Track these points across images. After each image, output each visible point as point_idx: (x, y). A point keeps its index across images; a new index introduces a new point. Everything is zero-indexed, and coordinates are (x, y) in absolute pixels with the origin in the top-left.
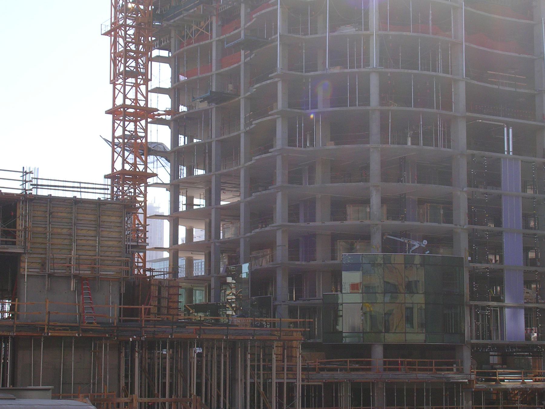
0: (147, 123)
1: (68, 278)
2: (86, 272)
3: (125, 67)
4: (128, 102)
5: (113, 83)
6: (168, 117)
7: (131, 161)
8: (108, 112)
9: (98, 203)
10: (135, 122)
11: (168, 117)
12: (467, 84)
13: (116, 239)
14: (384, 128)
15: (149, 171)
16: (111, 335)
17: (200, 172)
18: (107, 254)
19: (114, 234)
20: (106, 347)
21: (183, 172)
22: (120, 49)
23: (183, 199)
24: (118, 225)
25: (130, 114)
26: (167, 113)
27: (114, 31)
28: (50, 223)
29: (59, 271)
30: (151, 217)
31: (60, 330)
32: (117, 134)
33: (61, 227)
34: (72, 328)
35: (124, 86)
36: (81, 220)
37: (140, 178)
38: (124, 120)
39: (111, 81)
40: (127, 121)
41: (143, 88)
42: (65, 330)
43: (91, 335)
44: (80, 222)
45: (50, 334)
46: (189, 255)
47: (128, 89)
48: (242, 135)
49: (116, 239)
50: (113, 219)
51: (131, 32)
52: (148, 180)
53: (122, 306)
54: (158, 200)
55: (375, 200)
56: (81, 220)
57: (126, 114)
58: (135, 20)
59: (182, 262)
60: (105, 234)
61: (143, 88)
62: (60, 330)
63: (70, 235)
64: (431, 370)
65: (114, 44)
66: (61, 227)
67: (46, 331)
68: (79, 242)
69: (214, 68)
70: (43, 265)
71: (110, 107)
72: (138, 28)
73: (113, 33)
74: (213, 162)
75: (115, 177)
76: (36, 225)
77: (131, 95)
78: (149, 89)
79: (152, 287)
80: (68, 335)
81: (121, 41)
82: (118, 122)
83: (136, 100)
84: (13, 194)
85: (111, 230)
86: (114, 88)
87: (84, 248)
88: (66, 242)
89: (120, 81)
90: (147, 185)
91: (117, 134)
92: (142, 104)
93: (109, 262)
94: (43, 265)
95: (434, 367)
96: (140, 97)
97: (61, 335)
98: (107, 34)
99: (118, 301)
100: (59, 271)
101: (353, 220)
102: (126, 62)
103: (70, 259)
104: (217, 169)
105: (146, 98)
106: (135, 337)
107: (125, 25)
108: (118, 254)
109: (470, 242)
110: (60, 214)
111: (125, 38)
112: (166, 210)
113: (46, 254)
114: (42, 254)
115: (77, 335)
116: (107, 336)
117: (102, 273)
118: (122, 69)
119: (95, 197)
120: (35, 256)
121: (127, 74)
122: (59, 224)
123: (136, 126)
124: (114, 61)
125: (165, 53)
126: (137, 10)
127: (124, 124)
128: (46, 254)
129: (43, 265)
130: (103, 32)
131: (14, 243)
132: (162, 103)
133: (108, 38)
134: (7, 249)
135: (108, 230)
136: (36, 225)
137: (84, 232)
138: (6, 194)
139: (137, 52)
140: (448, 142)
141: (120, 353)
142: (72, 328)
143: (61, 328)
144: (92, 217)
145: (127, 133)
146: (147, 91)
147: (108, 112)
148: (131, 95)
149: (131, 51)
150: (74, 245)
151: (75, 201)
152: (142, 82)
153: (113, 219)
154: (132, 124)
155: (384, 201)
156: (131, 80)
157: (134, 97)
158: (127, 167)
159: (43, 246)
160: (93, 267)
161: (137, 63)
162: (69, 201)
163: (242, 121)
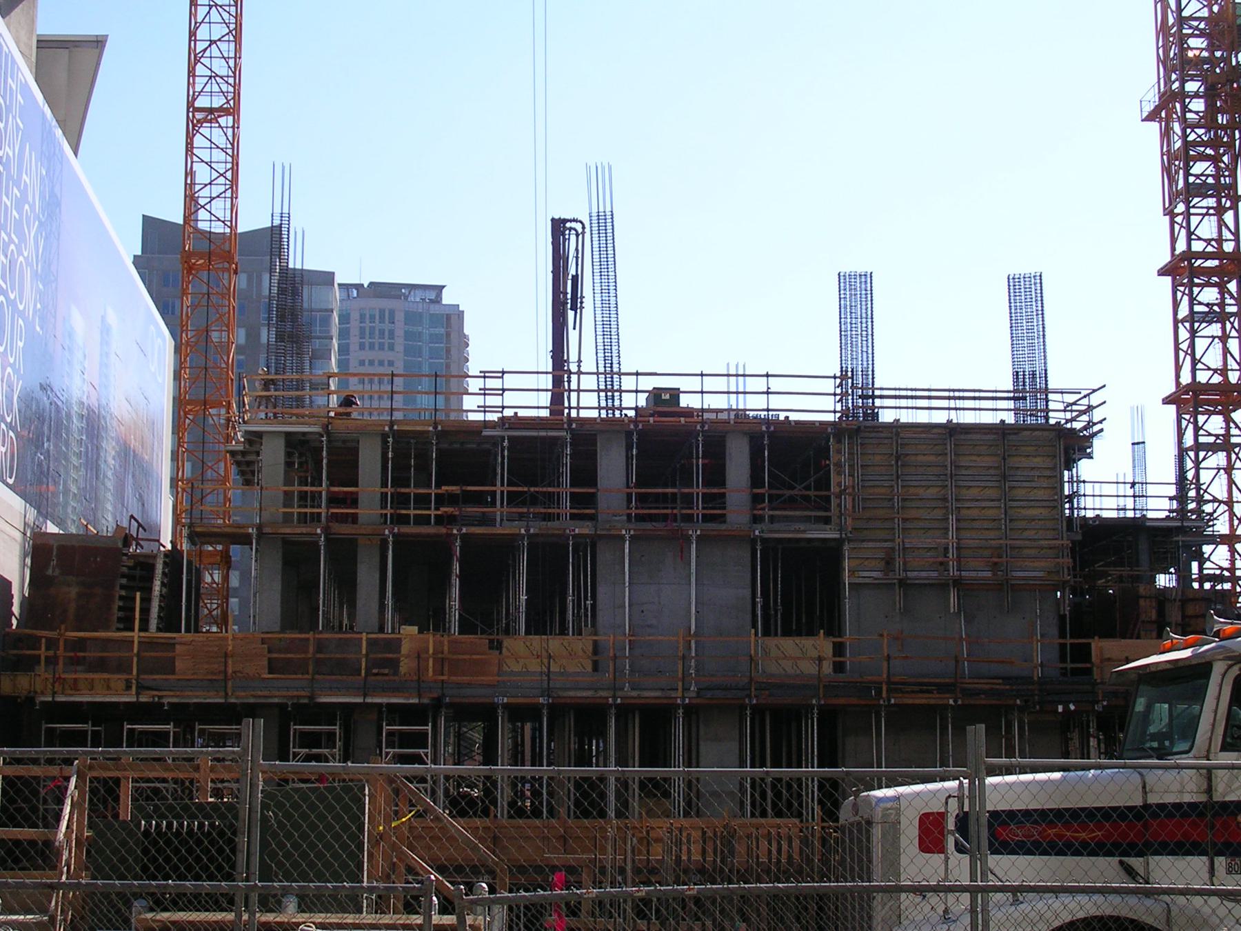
1: (941, 587)
2: (981, 574)
5: (1170, 213)
13: (1044, 504)
16: (1026, 701)
18: (1026, 534)
19: (1042, 492)
20: (1021, 728)
24: (1048, 473)
25: (1209, 272)
27: (1165, 108)
28: (898, 478)
29: (924, 574)
31: (913, 692)
33: (923, 483)
34: (943, 688)
35: (1187, 215)
36: (967, 468)
38: (1191, 285)
39: (1165, 209)
40: (1198, 285)
42: (922, 691)
43: (984, 702)
44: (964, 472)
45: (893, 701)
47: (1194, 220)
49: (1044, 504)
50: (1038, 461)
51: (1198, 105)
53: (1069, 641)
56: (967, 468)
57: (1195, 272)
58: (1204, 82)
60: (1020, 493)
62: (913, 692)
63: (945, 499)
65: (1166, 134)
66: (923, 483)
67: (884, 694)
68: (964, 512)
70: (888, 563)
72: (1210, 95)
73: (1163, 114)
76: (871, 483)
79: (1142, 602)
80: (932, 702)
81: (1177, 127)
82: (1182, 289)
84: (813, 423)
85: (1033, 484)
86: (1172, 223)
87: (977, 525)
88: (938, 514)
93: (1033, 552)
94: (889, 562)
95: (503, 768)
96: (1227, 234)
97: (917, 701)
98: (1151, 117)
99: (1054, 631)
100: (924, 574)
103: (946, 549)
106: (1072, 707)
107: (1182, 95)
108: (1050, 534)
110: (920, 458)
111: (1183, 121)
113: (893, 540)
114: (886, 541)
115: (951, 702)
116: (1018, 702)
117: (1014, 574)
118: (1181, 184)
120: (871, 545)
121: (1200, 190)
122: (919, 478)
123: (1222, 293)
124: (1167, 170)
126: (1212, 61)
127: (1191, 292)
128: (893, 540)
129: (889, 562)
130: (1145, 114)
131: (827, 521)
133: (1154, 127)
134: (804, 532)
135: (1025, 484)
136: (871, 483)
137: (973, 493)
138: (797, 422)
139: (1214, 143)
142: (943, 688)
143: (916, 688)
144: (988, 461)
145: (1197, 308)
150: (952, 519)
151: (952, 430)
152: (1228, 204)
153: (1038, 461)
156: (1215, 329)
157: (1215, 236)
158: (1202, 377)
159: (888, 525)
160: (996, 564)
161: (1217, 168)
162: (939, 431)
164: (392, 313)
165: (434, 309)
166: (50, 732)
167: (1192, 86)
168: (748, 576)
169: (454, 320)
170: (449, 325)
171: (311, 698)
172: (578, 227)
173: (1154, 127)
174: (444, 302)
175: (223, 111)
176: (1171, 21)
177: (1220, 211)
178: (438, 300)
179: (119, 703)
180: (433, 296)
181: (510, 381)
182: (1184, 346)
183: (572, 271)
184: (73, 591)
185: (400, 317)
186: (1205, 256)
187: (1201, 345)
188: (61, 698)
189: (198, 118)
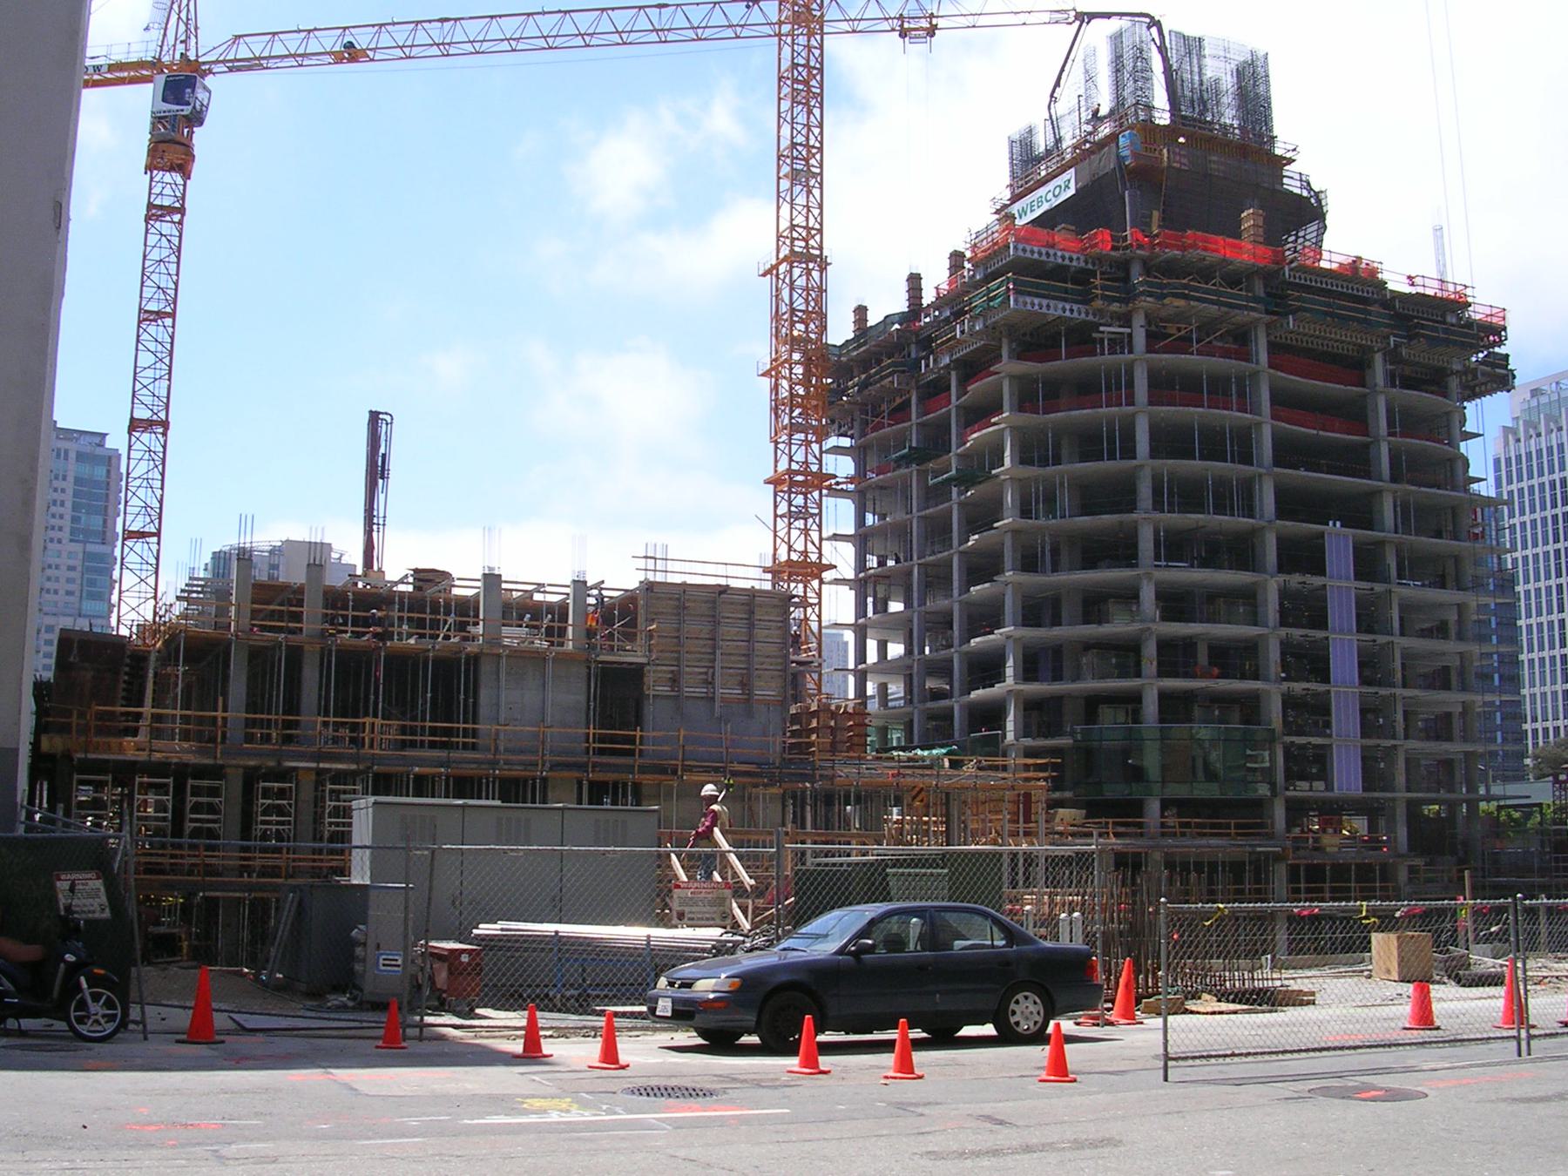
0: (821, 495)
3: (791, 418)
4: (795, 466)
6: (851, 487)
7: (802, 548)
8: (768, 482)
9: (752, 593)
10: (805, 495)
11: (851, 487)
12: (1273, 427)
14: (1157, 492)
15: (824, 561)
17: (896, 607)
21: (872, 561)
22: (784, 393)
23: (872, 646)
26: (851, 480)
27: (773, 372)
30: (829, 539)
32: (779, 512)
37: (811, 569)
38: (790, 492)
41: (815, 447)
46: (883, 679)
47: (794, 448)
48: (955, 507)
51: (799, 370)
52: (824, 575)
54: (838, 605)
55: (1148, 594)
57: (793, 483)
58: (805, 353)
59: (871, 689)
61: (815, 447)
64: (1229, 835)
65: (775, 388)
69: (914, 416)
71: (770, 473)
74: (915, 595)
75: (777, 571)
77: (799, 457)
78: (825, 535)
81: (785, 383)
83: (805, 553)
89: (784, 438)
90: (821, 582)
91: (779, 512)
92: (815, 468)
101: (1118, 626)
102: (792, 411)
104: (922, 603)
105: (820, 549)
107: (789, 361)
109: (1283, 654)
112: (849, 616)
118: (786, 421)
119: (747, 585)
123: (806, 499)
124: (775, 410)
125: (846, 442)
132: (843, 558)
140: (1249, 511)
141: (784, 806)
146: (821, 452)
147: (768, 482)
148: (799, 457)
149: (798, 395)
154: (801, 497)
155: (1160, 596)
156: (800, 524)
158: (794, 557)
163: (956, 584)
164: (66, 452)
165: (98, 451)
166: (1187, 923)
167: (796, 356)
168: (584, 688)
169: (114, 461)
170: (110, 465)
171: (279, 763)
172: (388, 418)
173: (766, 383)
174: (108, 445)
175: (168, 315)
176: (784, 309)
177: (808, 443)
178: (101, 445)
179: (107, 761)
180: (97, 440)
181: (671, 566)
182: (781, 534)
183: (382, 450)
184: (89, 675)
185: (72, 455)
186: (798, 473)
187: (795, 533)
188: (91, 756)
189: (147, 317)
